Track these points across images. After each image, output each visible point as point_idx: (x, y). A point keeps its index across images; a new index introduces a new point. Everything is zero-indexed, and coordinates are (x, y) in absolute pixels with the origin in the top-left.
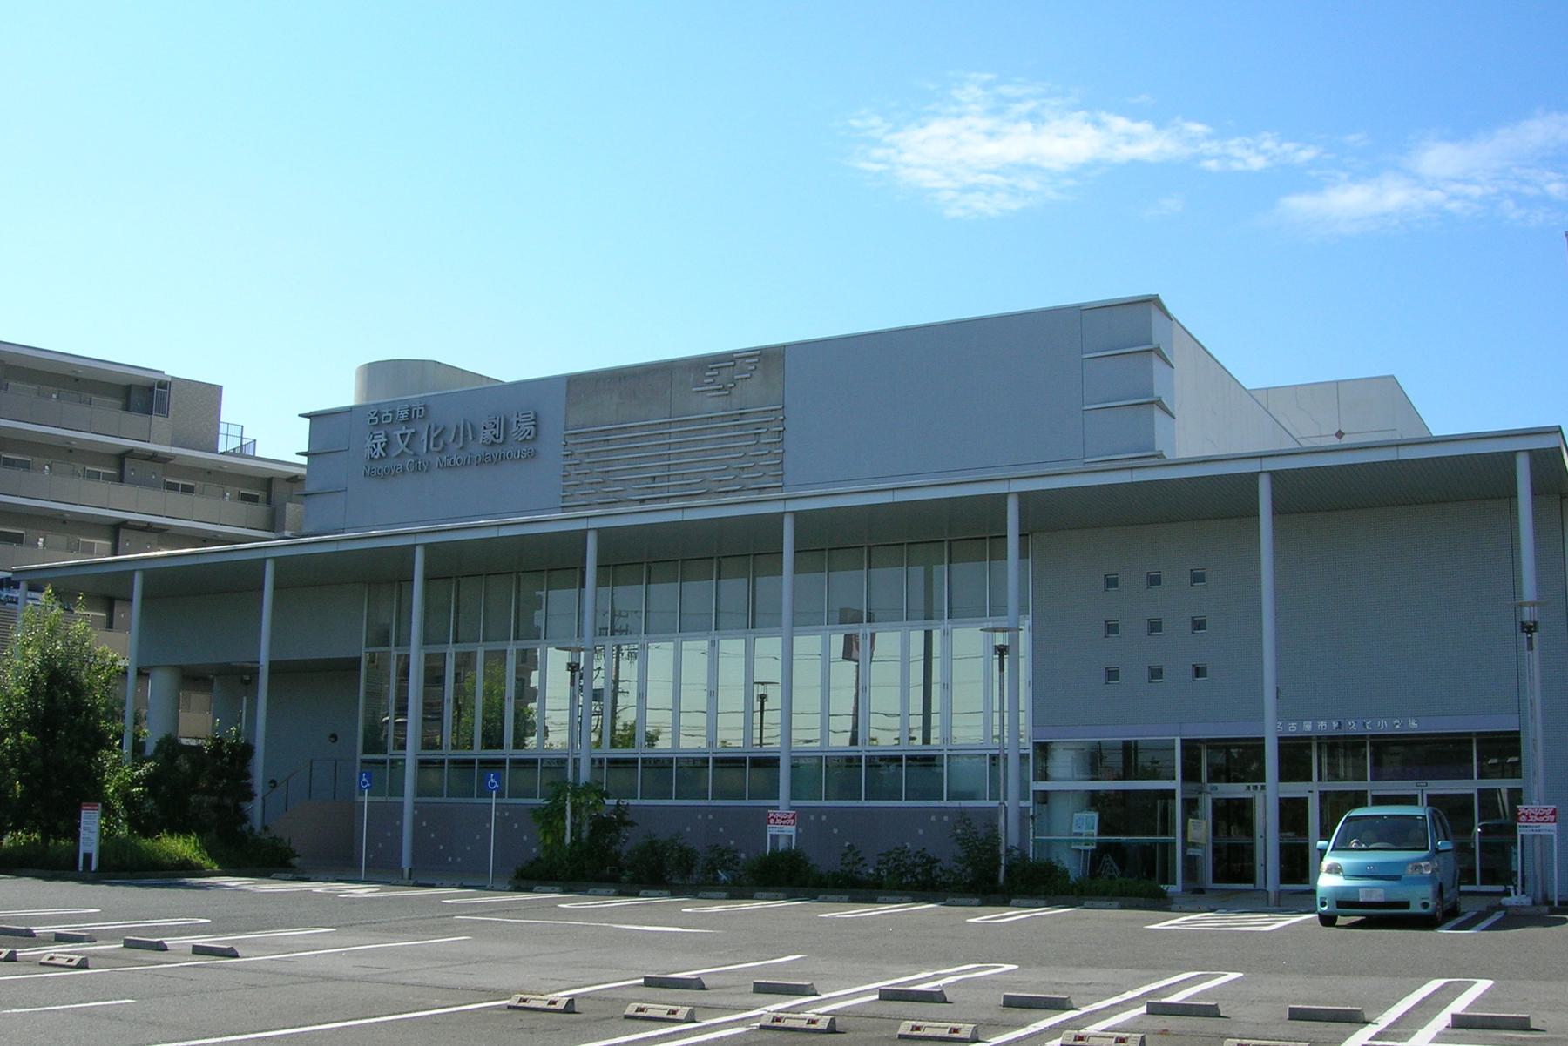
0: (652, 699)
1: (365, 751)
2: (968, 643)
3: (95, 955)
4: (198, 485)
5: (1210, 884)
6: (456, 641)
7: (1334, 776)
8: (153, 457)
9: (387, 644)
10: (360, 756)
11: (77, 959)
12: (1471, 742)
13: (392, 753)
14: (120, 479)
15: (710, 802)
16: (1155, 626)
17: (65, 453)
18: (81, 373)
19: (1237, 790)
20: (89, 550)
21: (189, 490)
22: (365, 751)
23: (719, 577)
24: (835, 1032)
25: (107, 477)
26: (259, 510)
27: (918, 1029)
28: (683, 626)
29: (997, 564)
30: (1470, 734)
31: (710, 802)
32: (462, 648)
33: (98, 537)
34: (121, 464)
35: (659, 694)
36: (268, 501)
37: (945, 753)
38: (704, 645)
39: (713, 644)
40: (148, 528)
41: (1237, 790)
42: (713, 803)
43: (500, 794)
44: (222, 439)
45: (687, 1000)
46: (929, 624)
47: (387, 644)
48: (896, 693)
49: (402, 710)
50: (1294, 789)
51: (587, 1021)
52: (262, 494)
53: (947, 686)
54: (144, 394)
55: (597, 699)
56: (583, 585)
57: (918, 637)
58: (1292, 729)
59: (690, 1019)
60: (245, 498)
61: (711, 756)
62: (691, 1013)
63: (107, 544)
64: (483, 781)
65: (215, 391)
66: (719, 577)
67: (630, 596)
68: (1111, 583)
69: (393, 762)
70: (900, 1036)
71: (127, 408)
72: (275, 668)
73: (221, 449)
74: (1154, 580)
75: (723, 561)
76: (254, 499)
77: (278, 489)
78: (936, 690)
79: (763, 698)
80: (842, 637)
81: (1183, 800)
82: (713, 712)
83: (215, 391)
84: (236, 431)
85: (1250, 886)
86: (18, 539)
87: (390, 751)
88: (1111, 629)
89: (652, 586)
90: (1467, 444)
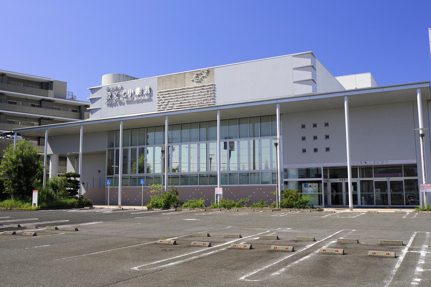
0: (183, 161)
1: (108, 175)
2: (266, 142)
3: (38, 232)
4: (62, 108)
5: (331, 205)
6: (131, 146)
7: (363, 177)
8: (49, 101)
9: (113, 147)
10: (107, 176)
11: (33, 233)
12: (402, 167)
13: (115, 175)
14: (41, 107)
15: (228, 185)
16: (315, 138)
17: (26, 100)
18: (29, 79)
19: (337, 180)
20: (33, 125)
21: (59, 109)
22: (108, 175)
23: (200, 128)
24: (176, 244)
25: (37, 106)
26: (77, 114)
27: (337, 251)
28: (190, 140)
29: (273, 122)
30: (401, 165)
31: (228, 185)
32: (133, 147)
33: (36, 122)
34: (40, 103)
35: (185, 160)
36: (80, 112)
37: (260, 172)
38: (187, 146)
39: (198, 145)
40: (49, 119)
41: (337, 180)
42: (130, 187)
43: (144, 185)
44: (67, 96)
45: (208, 240)
46: (208, 142)
47: (113, 147)
48: (247, 157)
49: (117, 164)
50: (355, 180)
51: (180, 247)
52: (78, 110)
53: (260, 154)
54: (47, 85)
55: (166, 159)
56: (164, 130)
57: (252, 142)
58: (355, 164)
59: (210, 246)
60: (73, 111)
61: (260, 172)
62: (210, 244)
63: (38, 123)
64: (139, 181)
65: (66, 83)
66: (181, 129)
67: (176, 133)
68: (303, 126)
69: (115, 177)
70: (369, 256)
71: (42, 88)
72: (84, 154)
73: (67, 98)
74: (315, 126)
75: (261, 117)
76: (76, 111)
77: (82, 108)
78: (257, 157)
79: (211, 159)
80: (253, 140)
81: (324, 183)
82: (199, 164)
83: (66, 83)
84: (71, 94)
85: (342, 206)
86: (14, 123)
87: (114, 174)
88: (304, 139)
89: (229, 126)
90: (405, 86)
